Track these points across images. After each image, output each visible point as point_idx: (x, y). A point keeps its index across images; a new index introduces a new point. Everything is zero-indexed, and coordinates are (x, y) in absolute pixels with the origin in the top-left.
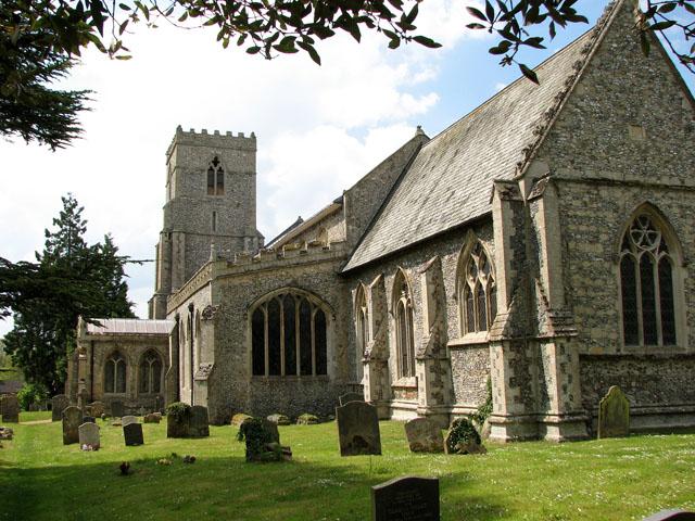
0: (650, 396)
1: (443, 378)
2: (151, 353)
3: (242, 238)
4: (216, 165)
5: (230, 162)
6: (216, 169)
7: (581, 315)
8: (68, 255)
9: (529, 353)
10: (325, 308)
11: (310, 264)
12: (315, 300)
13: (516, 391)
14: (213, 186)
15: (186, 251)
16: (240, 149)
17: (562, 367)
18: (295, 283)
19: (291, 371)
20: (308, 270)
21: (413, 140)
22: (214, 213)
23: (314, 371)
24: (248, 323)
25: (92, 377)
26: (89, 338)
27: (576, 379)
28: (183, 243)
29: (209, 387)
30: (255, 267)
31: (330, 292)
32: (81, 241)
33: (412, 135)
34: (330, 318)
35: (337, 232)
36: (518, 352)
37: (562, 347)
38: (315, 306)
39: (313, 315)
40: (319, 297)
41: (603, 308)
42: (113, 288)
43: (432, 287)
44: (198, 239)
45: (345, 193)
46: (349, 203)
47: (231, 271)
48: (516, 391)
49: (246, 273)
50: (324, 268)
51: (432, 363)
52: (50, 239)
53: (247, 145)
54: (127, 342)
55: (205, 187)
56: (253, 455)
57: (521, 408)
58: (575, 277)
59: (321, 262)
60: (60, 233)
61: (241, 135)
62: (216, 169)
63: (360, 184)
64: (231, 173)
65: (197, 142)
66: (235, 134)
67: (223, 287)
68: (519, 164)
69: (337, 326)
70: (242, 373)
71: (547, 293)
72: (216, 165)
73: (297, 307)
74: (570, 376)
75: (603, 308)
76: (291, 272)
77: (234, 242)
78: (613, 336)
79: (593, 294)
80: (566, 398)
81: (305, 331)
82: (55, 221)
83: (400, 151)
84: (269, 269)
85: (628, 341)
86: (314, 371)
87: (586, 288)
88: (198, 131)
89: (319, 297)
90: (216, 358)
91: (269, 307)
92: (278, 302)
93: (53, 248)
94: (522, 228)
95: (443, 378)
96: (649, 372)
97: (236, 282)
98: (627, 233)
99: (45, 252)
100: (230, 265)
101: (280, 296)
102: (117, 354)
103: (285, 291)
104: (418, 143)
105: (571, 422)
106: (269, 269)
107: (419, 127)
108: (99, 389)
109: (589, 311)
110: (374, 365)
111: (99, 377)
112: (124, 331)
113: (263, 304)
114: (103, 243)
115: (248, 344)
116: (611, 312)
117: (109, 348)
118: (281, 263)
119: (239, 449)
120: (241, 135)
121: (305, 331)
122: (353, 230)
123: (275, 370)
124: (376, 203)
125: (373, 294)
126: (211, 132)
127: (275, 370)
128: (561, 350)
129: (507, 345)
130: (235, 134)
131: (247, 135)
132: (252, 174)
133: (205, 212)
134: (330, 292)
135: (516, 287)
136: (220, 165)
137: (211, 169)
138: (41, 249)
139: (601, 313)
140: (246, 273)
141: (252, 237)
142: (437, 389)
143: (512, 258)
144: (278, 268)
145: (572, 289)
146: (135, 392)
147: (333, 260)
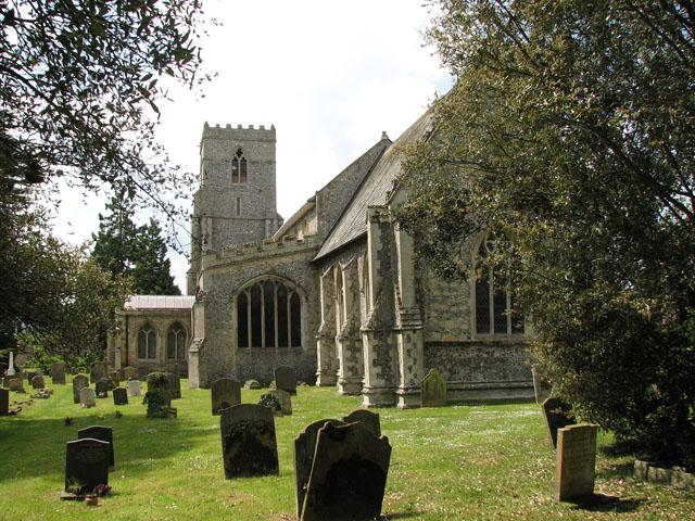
0: (496, 374)
1: (358, 355)
2: (177, 326)
3: (264, 220)
4: (239, 156)
5: (251, 154)
6: (240, 159)
7: (437, 311)
8: (120, 235)
9: (390, 341)
10: (299, 291)
11: (286, 254)
12: (291, 285)
13: (378, 370)
14: (237, 175)
15: (213, 233)
16: (261, 140)
17: (408, 352)
18: (273, 271)
19: (270, 343)
20: (284, 260)
21: (378, 145)
22: (238, 199)
23: (290, 344)
24: (234, 305)
25: (127, 346)
26: (124, 313)
27: (420, 361)
28: (211, 226)
29: (200, 357)
30: (239, 259)
31: (303, 278)
32: (131, 222)
33: (378, 139)
34: (303, 299)
35: (313, 226)
36: (381, 339)
37: (409, 337)
38: (291, 290)
39: (289, 297)
40: (294, 282)
41: (457, 305)
42: (157, 265)
43: (379, 279)
44: (224, 223)
45: (317, 193)
46: (321, 200)
47: (219, 262)
48: (378, 370)
49: (233, 263)
50: (297, 257)
51: (348, 343)
52: (103, 222)
53: (267, 137)
54: (156, 316)
55: (229, 176)
56: (151, 414)
57: (382, 382)
58: (432, 281)
59: (296, 252)
60: (112, 216)
61: (262, 128)
62: (240, 159)
63: (329, 185)
64: (253, 163)
65: (221, 136)
66: (256, 127)
67: (213, 276)
68: (388, 193)
69: (309, 306)
70: (229, 345)
71: (401, 296)
72: (239, 156)
73: (275, 291)
74: (415, 360)
75: (457, 305)
76: (270, 262)
77: (257, 224)
78: (465, 327)
79: (448, 294)
80: (411, 376)
81: (282, 313)
82: (107, 206)
83: (366, 154)
84: (251, 260)
85: (479, 330)
86: (290, 344)
87: (441, 289)
88: (223, 126)
89: (294, 282)
90: (206, 333)
91: (252, 291)
92: (259, 288)
93: (106, 230)
94: (388, 243)
95: (358, 355)
96: (496, 355)
97: (224, 271)
98: (483, 243)
99: (100, 233)
100: (218, 257)
101: (261, 282)
102: (147, 326)
103: (265, 277)
104: (382, 147)
105: (415, 394)
106: (251, 260)
107: (384, 133)
108: (133, 356)
109: (444, 307)
110: (324, 342)
111: (133, 346)
112: (155, 307)
113: (247, 289)
114: (149, 225)
115: (234, 322)
116: (463, 308)
117: (141, 321)
118: (262, 254)
119: (144, 410)
120: (262, 128)
121: (282, 313)
122: (323, 225)
123: (256, 343)
124: (344, 201)
125: (324, 283)
126: (234, 127)
127: (256, 343)
128: (408, 340)
129: (372, 335)
130: (256, 127)
131: (268, 128)
132: (272, 162)
133: (231, 197)
134: (303, 278)
135: (380, 290)
136: (242, 156)
137: (235, 160)
138: (97, 231)
139: (454, 309)
140: (233, 263)
141: (272, 220)
142: (353, 364)
143: (378, 267)
144: (258, 259)
145: (429, 290)
146: (163, 358)
147: (306, 251)
